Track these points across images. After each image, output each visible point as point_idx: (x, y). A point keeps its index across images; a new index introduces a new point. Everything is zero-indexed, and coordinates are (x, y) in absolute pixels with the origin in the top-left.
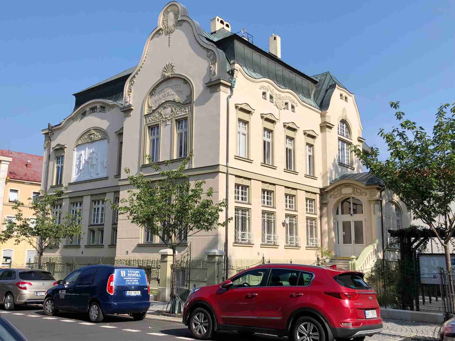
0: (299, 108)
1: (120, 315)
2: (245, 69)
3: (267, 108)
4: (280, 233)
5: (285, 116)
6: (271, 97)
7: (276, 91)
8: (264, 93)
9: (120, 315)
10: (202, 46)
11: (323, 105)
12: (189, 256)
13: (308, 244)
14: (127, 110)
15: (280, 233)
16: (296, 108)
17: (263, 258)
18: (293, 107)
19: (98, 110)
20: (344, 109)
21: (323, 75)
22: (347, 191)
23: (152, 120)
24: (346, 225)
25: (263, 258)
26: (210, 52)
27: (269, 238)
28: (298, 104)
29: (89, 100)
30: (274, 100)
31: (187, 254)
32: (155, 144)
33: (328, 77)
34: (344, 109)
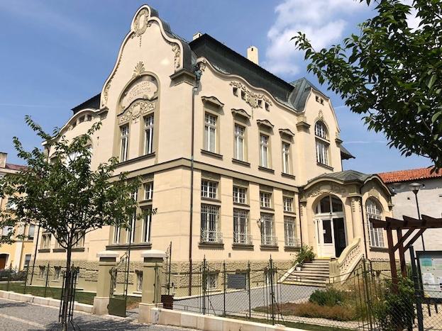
0: (273, 108)
1: (416, 264)
2: (216, 67)
3: (239, 104)
4: (254, 233)
5: (258, 114)
6: (243, 94)
7: (247, 89)
8: (235, 90)
9: (416, 264)
10: (164, 38)
11: (299, 109)
12: (169, 260)
13: (235, 241)
14: (104, 113)
15: (254, 233)
16: (270, 107)
17: (205, 260)
18: (267, 106)
19: (86, 119)
20: (321, 111)
21: (299, 81)
22: (325, 190)
23: (123, 120)
24: (326, 224)
25: (205, 260)
26: (176, 46)
27: (268, 239)
28: (272, 103)
29: (82, 109)
30: (246, 97)
31: (125, 256)
32: (125, 143)
33: (304, 82)
34: (321, 111)
